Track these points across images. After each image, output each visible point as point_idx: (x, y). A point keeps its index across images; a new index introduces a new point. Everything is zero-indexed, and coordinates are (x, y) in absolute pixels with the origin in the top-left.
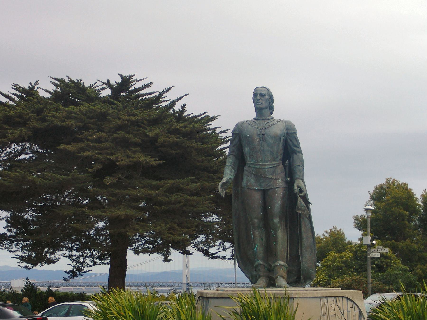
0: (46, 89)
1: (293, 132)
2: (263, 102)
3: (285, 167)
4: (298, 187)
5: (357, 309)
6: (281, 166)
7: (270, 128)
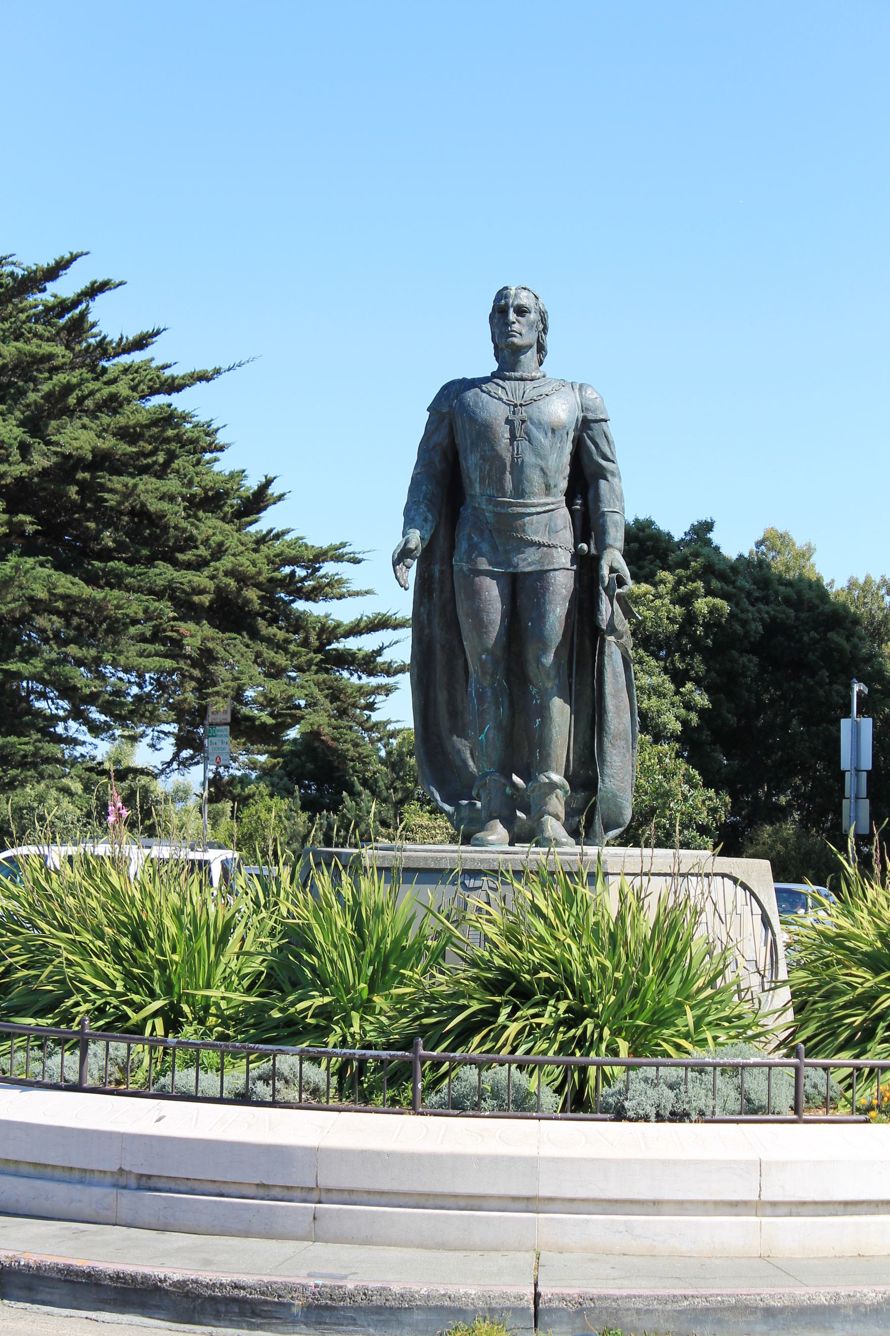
0: (32, 1264)
1: (602, 417)
2: (523, 332)
3: (572, 512)
4: (612, 570)
5: (757, 910)
6: (565, 511)
7: (540, 403)
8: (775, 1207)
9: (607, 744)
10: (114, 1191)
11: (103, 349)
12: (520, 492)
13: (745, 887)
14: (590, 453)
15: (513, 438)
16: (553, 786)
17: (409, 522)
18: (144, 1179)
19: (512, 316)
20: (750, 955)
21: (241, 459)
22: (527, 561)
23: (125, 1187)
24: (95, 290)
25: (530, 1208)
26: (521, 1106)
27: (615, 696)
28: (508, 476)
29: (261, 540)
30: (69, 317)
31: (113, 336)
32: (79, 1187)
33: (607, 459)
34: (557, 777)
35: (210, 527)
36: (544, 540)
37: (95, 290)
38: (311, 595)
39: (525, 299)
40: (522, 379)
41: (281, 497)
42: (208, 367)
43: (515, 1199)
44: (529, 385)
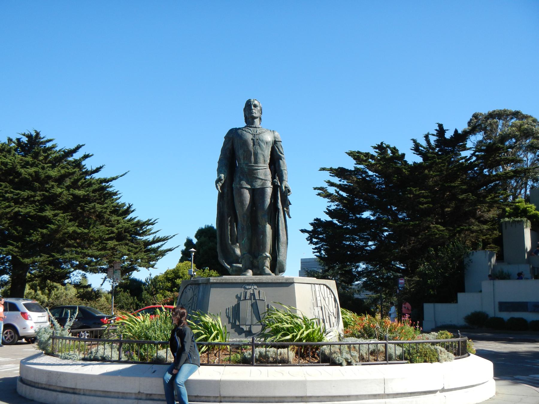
5: (333, 296)
8: (388, 396)
9: (280, 245)
10: (137, 401)
11: (87, 173)
12: (256, 162)
13: (329, 289)
14: (277, 152)
15: (254, 145)
16: (267, 257)
17: (219, 171)
18: (148, 396)
19: (253, 107)
20: (332, 311)
21: (124, 199)
22: (258, 184)
23: (140, 399)
24: (86, 157)
25: (303, 400)
26: (284, 362)
27: (282, 230)
28: (253, 157)
29: (130, 220)
30: (78, 164)
31: (90, 169)
32: (122, 400)
33: (282, 153)
34: (268, 255)
35: (114, 218)
36: (263, 178)
37: (86, 157)
38: (140, 235)
39: (256, 102)
40: (255, 127)
41: (133, 211)
42: (114, 176)
43: (297, 397)
44: (258, 129)
